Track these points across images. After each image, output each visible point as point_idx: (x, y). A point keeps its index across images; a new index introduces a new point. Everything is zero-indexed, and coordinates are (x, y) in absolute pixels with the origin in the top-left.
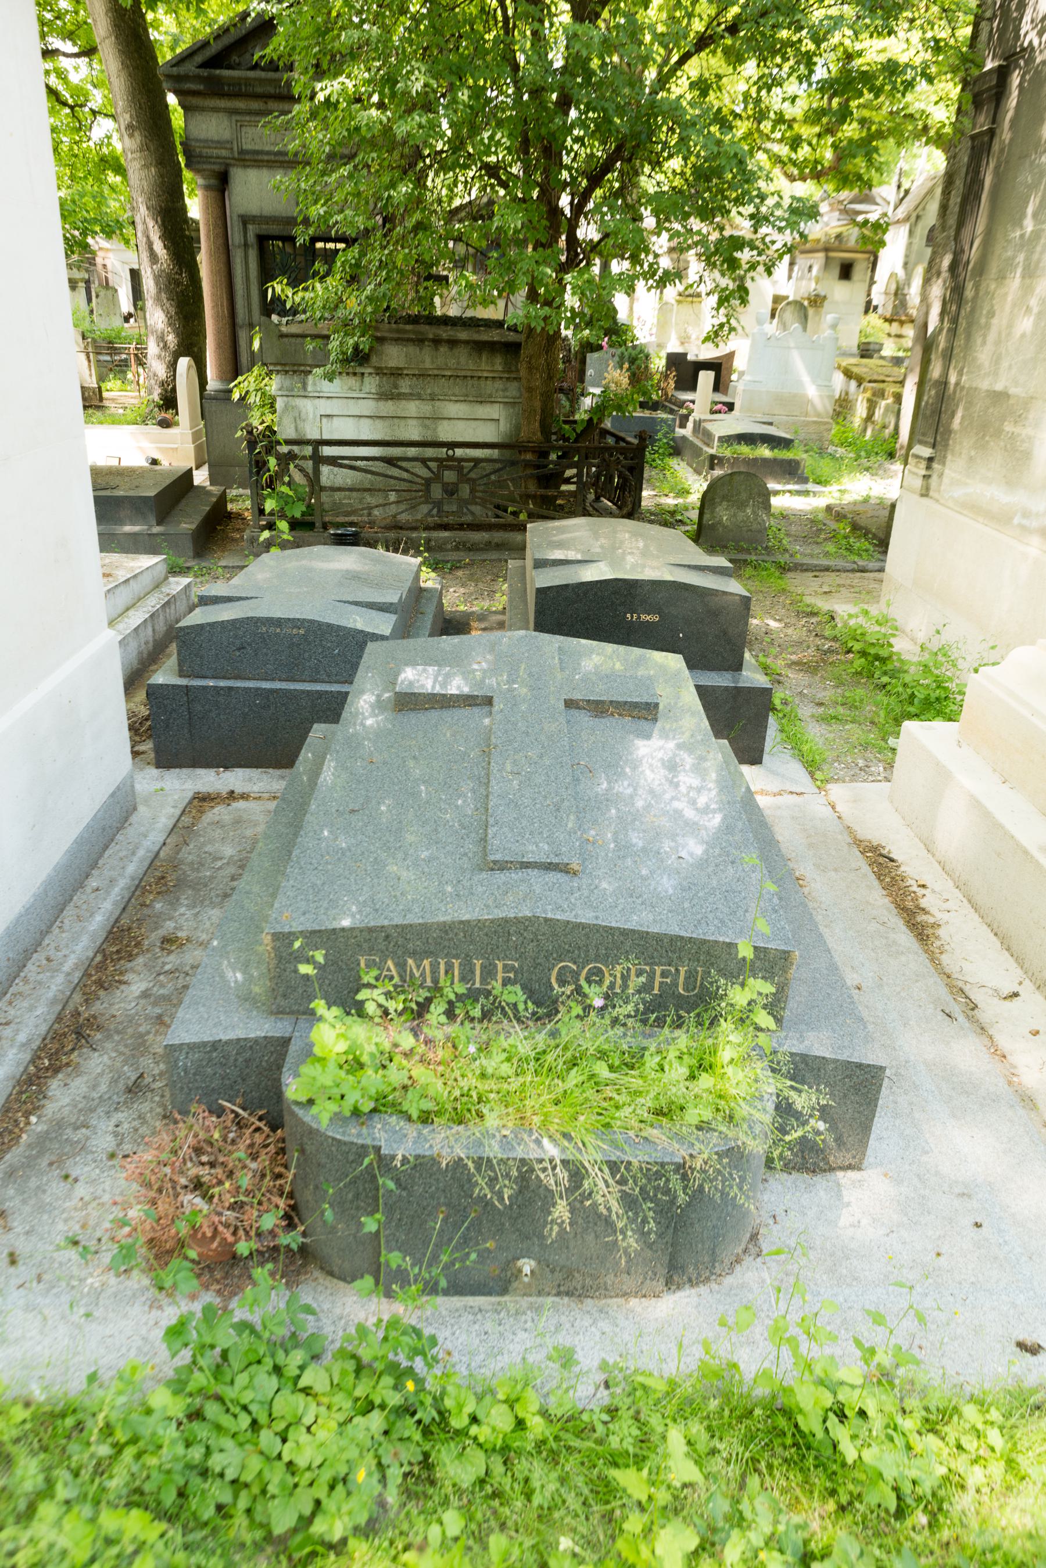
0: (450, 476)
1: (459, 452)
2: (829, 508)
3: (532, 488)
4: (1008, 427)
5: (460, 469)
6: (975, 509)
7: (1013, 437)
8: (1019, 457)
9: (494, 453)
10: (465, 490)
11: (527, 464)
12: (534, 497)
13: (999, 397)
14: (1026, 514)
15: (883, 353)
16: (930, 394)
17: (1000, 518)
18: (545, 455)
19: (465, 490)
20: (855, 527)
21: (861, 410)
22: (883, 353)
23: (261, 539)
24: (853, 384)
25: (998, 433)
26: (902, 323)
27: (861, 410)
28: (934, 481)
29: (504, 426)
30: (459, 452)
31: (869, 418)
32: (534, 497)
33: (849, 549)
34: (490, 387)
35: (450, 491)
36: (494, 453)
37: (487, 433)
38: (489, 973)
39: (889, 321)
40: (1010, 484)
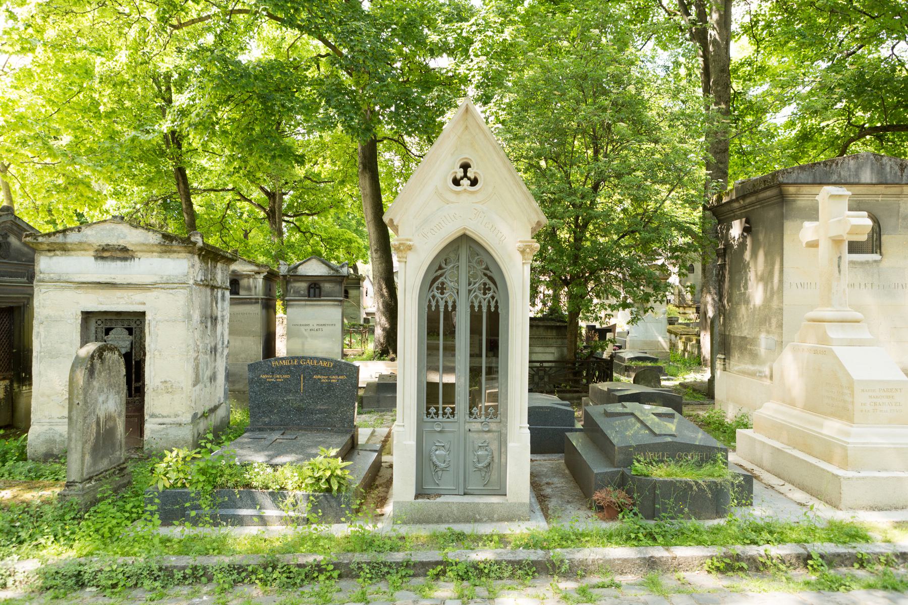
0: (541, 373)
1: (545, 365)
2: (680, 384)
3: (571, 377)
4: (748, 347)
5: (545, 371)
6: (744, 373)
7: (751, 350)
8: (754, 357)
9: (553, 364)
10: (546, 379)
11: (570, 368)
12: (572, 380)
13: (744, 338)
14: (760, 372)
15: (680, 321)
16: (717, 338)
17: (752, 374)
18: (574, 364)
19: (546, 379)
20: (694, 390)
21: (681, 347)
22: (680, 321)
23: (52, 493)
24: (673, 336)
25: (746, 349)
26: (684, 308)
27: (681, 347)
28: (727, 366)
29: (556, 355)
30: (545, 365)
31: (685, 350)
32: (572, 380)
33: (695, 397)
34: (551, 341)
35: (541, 378)
36: (553, 364)
37: (550, 357)
38: (663, 456)
39: (678, 307)
40: (753, 364)
